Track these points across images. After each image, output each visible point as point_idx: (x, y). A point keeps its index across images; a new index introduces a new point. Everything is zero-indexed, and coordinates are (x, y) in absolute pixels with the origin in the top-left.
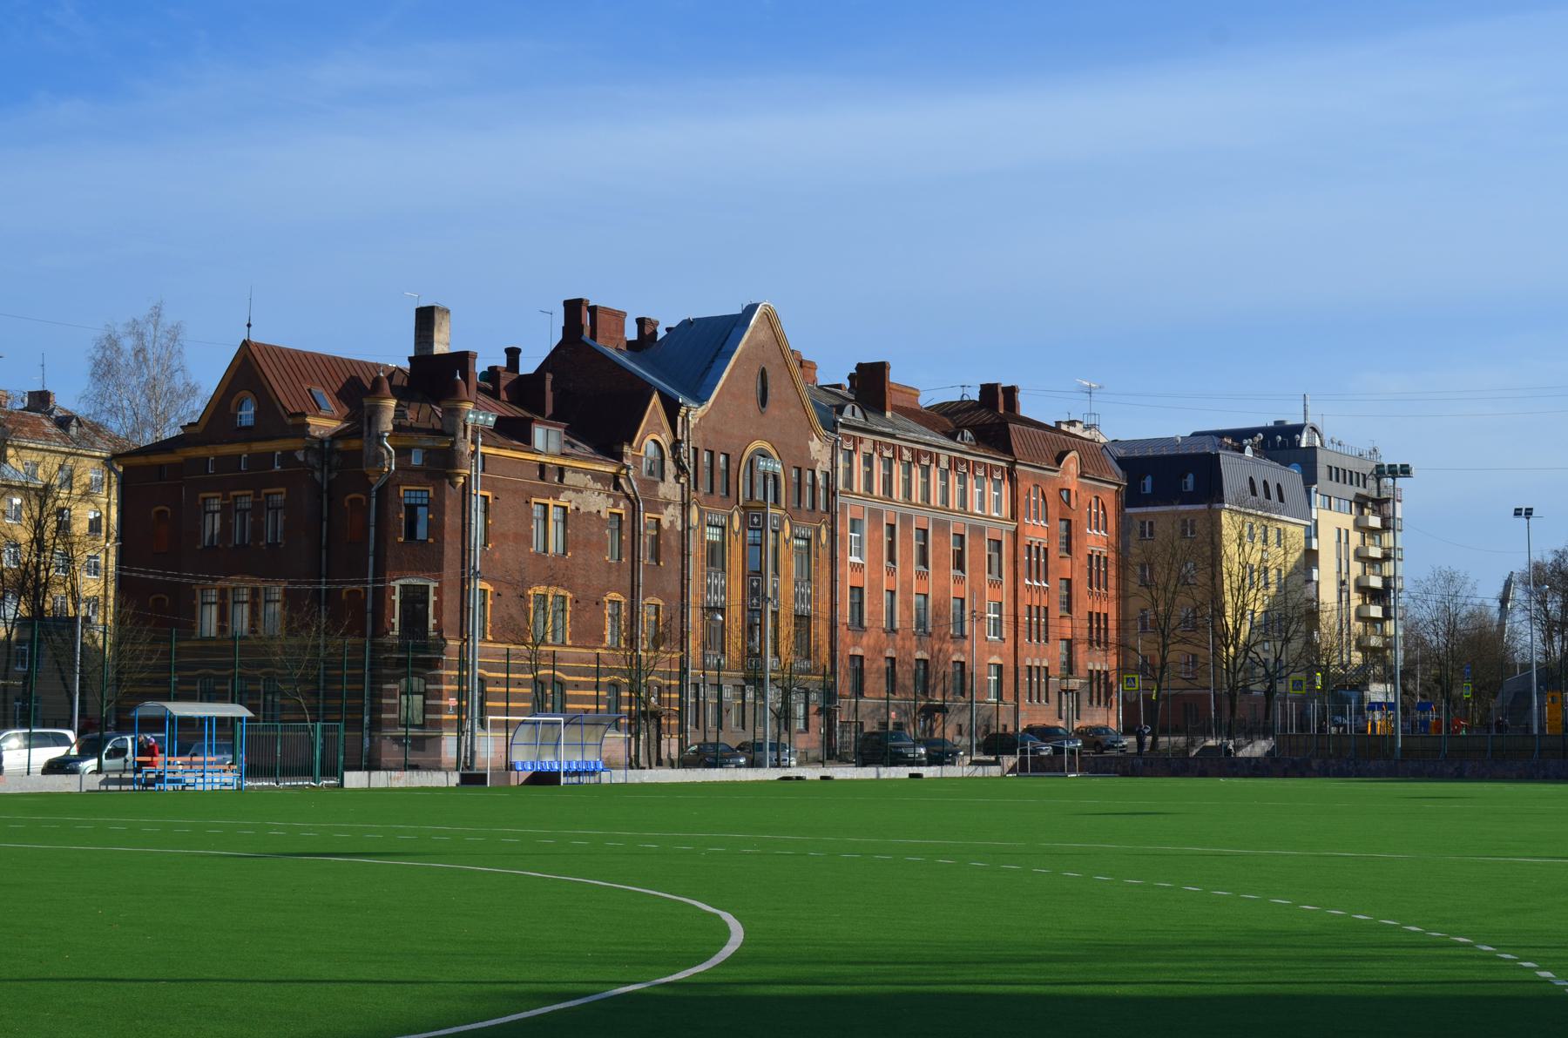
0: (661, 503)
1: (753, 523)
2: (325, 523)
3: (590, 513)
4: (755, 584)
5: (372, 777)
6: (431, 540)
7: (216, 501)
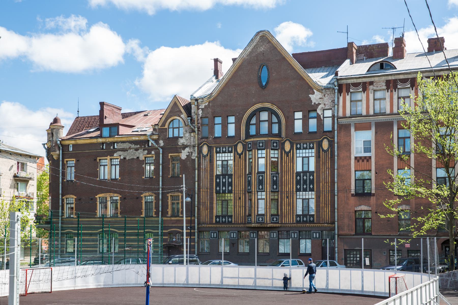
0: (180, 148)
1: (274, 146)
3: (133, 159)
4: (275, 187)
5: (209, 281)
7: (116, 160)
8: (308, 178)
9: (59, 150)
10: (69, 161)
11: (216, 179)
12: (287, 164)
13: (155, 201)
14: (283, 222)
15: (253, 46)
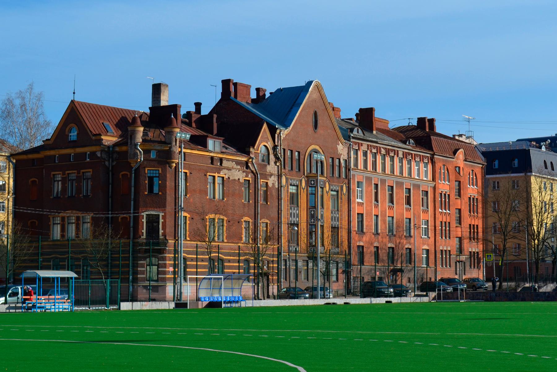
1: (311, 184)
2: (110, 186)
4: (312, 212)
5: (134, 305)
6: (160, 193)
10: (87, 172)
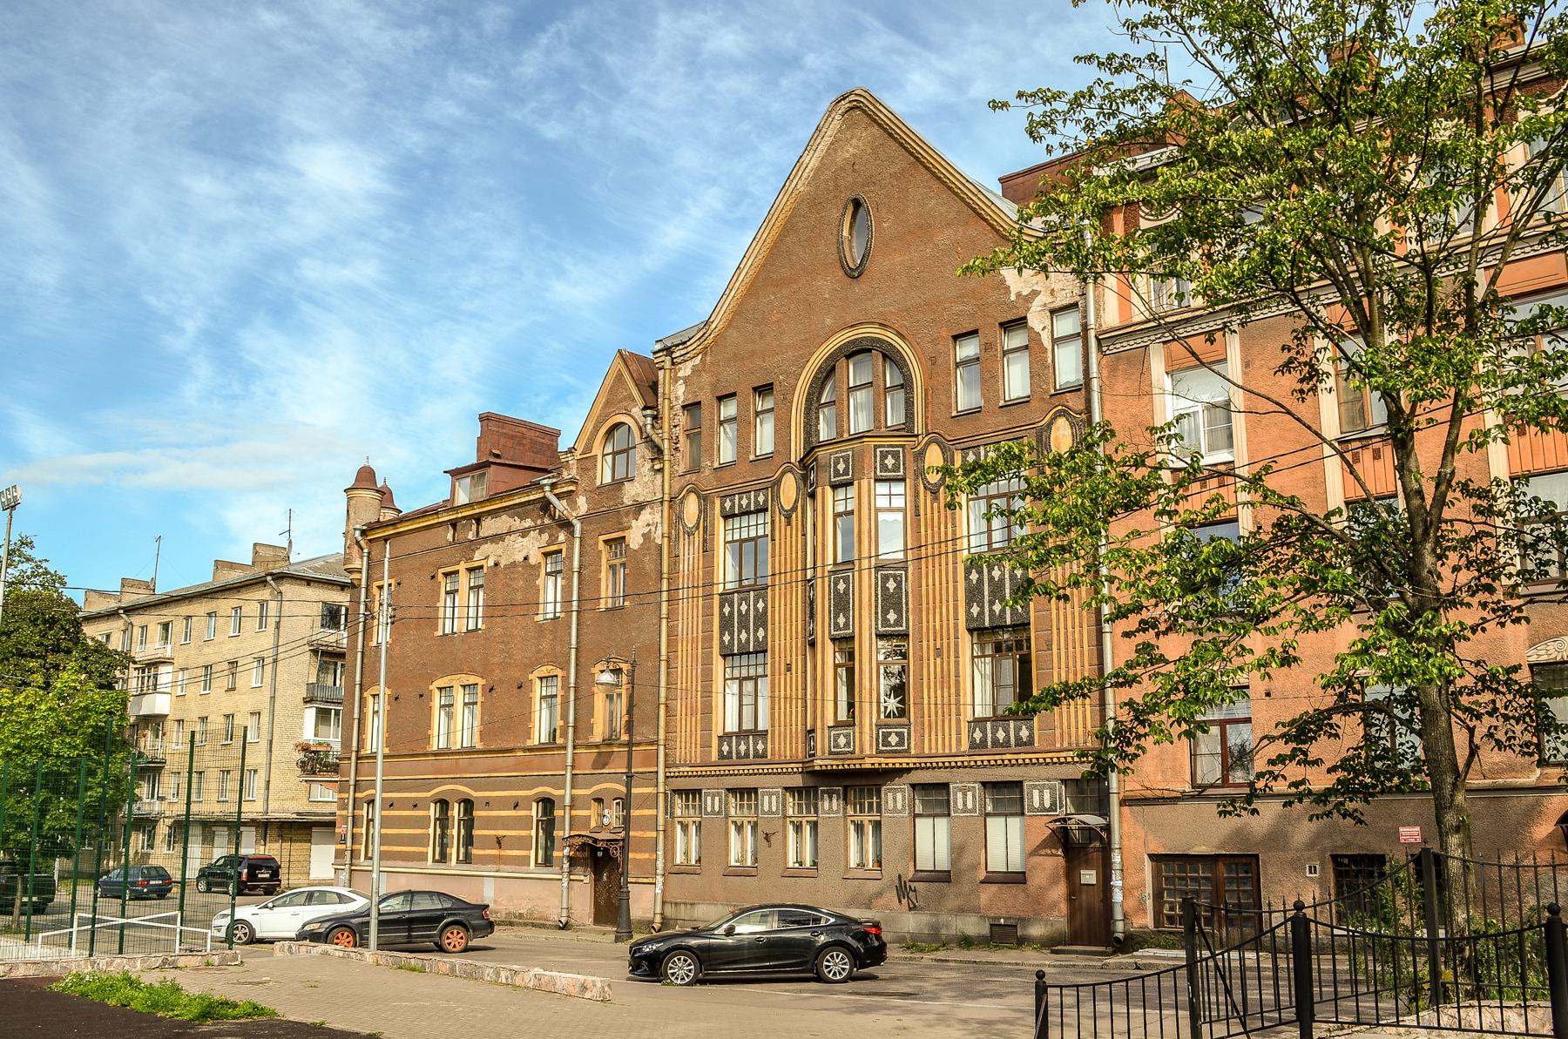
1: (884, 468)
8: (1007, 576)
9: (362, 558)
11: (722, 606)
12: (936, 529)
13: (389, 692)
14: (927, 751)
15: (823, 147)
